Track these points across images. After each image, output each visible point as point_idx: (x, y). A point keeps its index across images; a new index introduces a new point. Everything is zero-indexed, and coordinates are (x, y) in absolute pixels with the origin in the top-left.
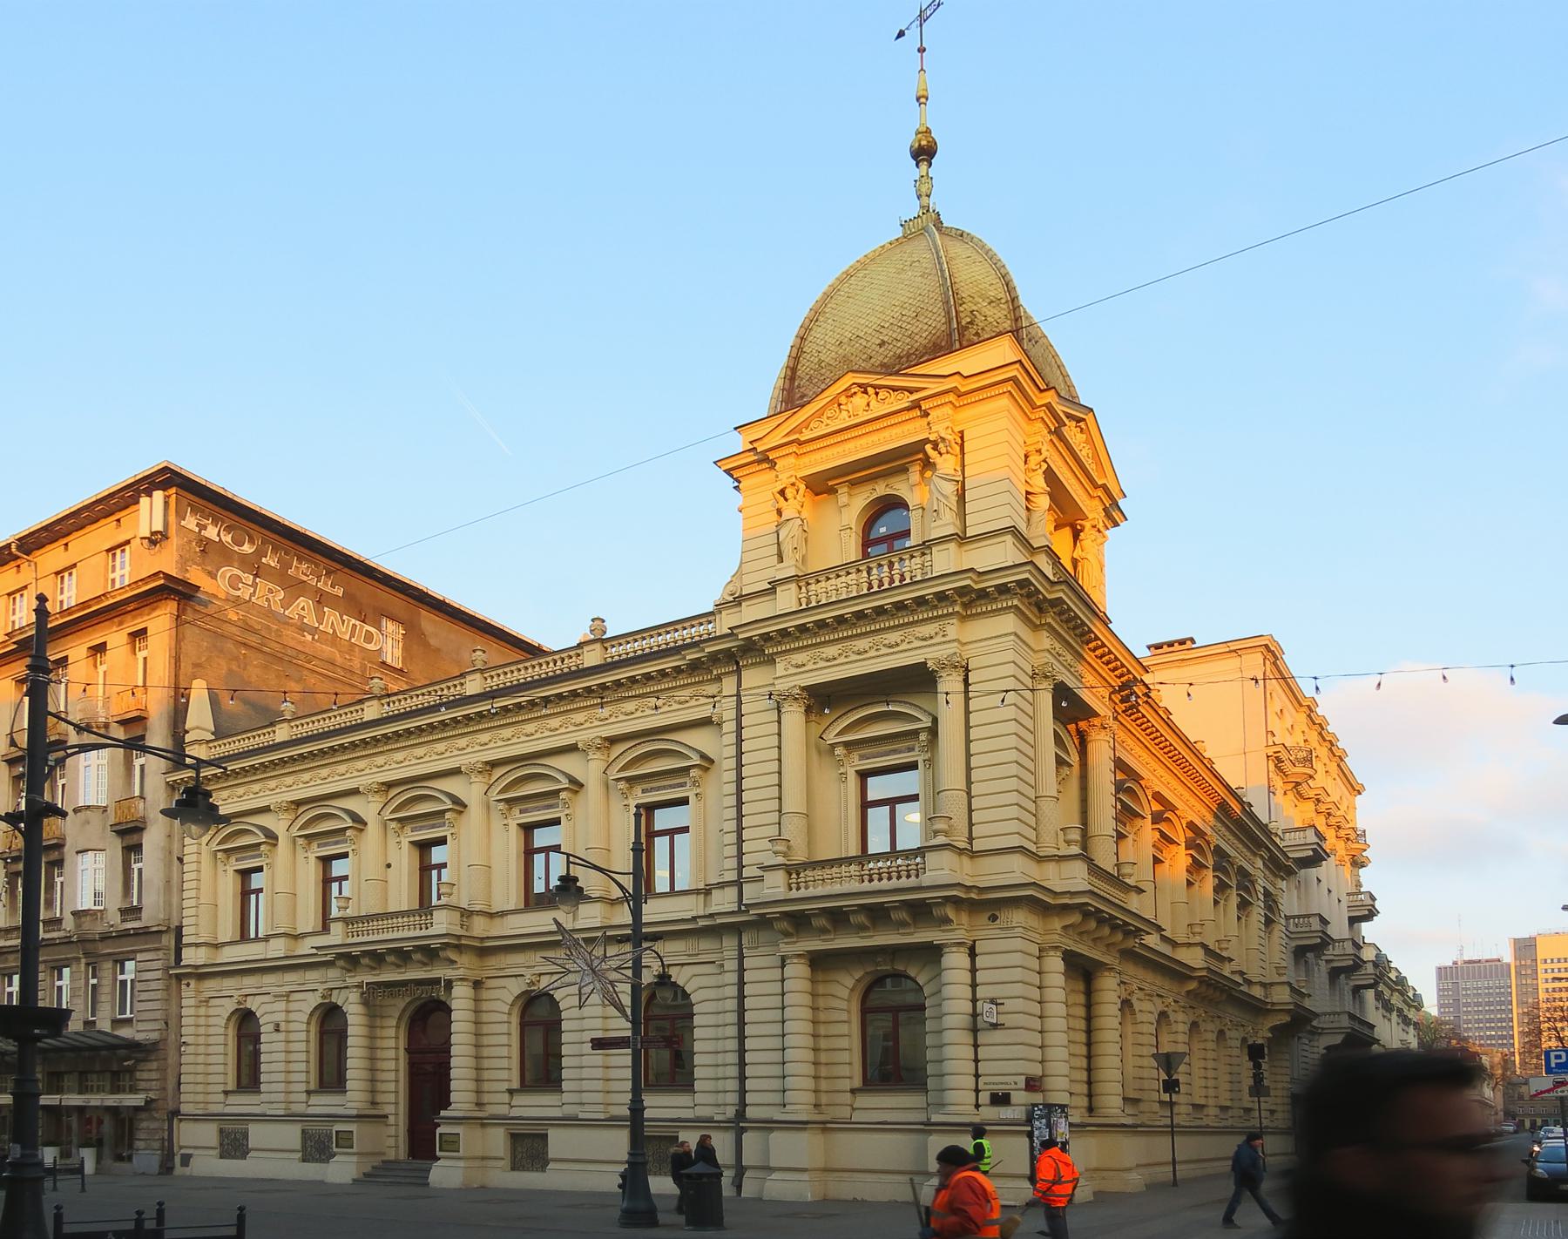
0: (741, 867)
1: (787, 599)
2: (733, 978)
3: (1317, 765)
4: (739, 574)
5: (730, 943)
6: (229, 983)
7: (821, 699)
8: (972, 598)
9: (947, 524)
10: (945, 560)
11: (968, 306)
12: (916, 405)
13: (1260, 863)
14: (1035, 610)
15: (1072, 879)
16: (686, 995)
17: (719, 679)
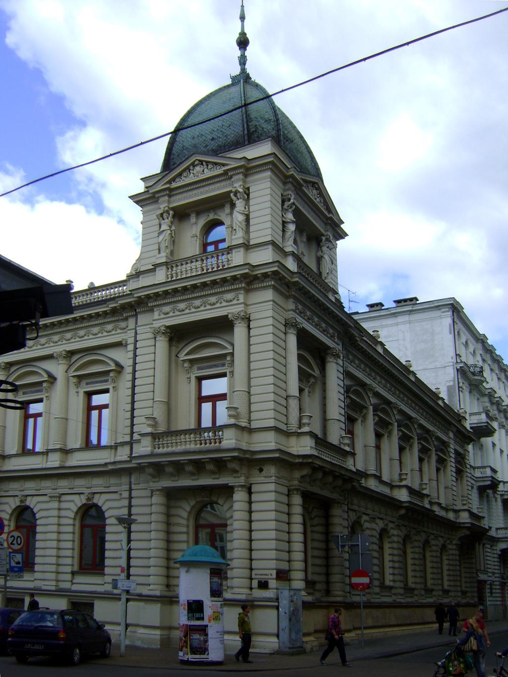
0: (132, 433)
1: (161, 276)
2: (126, 502)
3: (485, 374)
4: (139, 260)
5: (125, 480)
6: (80, 482)
7: (178, 335)
8: (250, 280)
9: (238, 238)
10: (238, 258)
11: (254, 123)
12: (226, 173)
13: (451, 435)
14: (285, 287)
15: (303, 447)
16: (34, 514)
17: (126, 319)
